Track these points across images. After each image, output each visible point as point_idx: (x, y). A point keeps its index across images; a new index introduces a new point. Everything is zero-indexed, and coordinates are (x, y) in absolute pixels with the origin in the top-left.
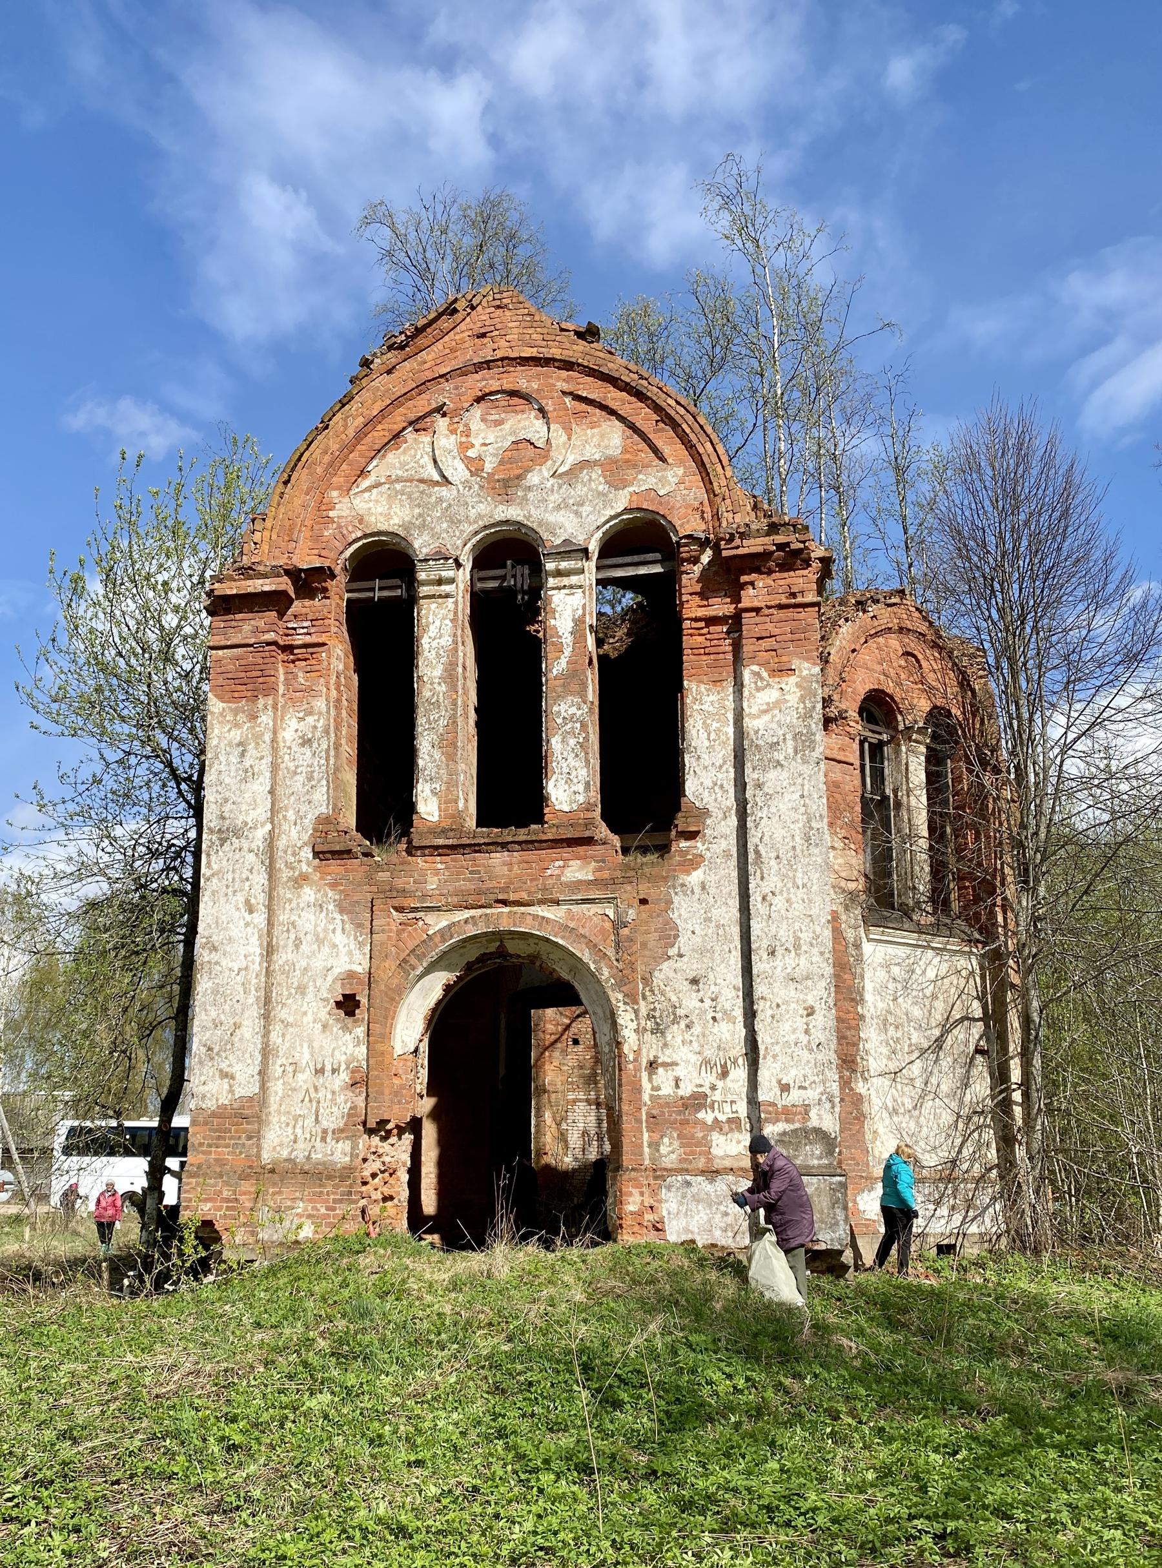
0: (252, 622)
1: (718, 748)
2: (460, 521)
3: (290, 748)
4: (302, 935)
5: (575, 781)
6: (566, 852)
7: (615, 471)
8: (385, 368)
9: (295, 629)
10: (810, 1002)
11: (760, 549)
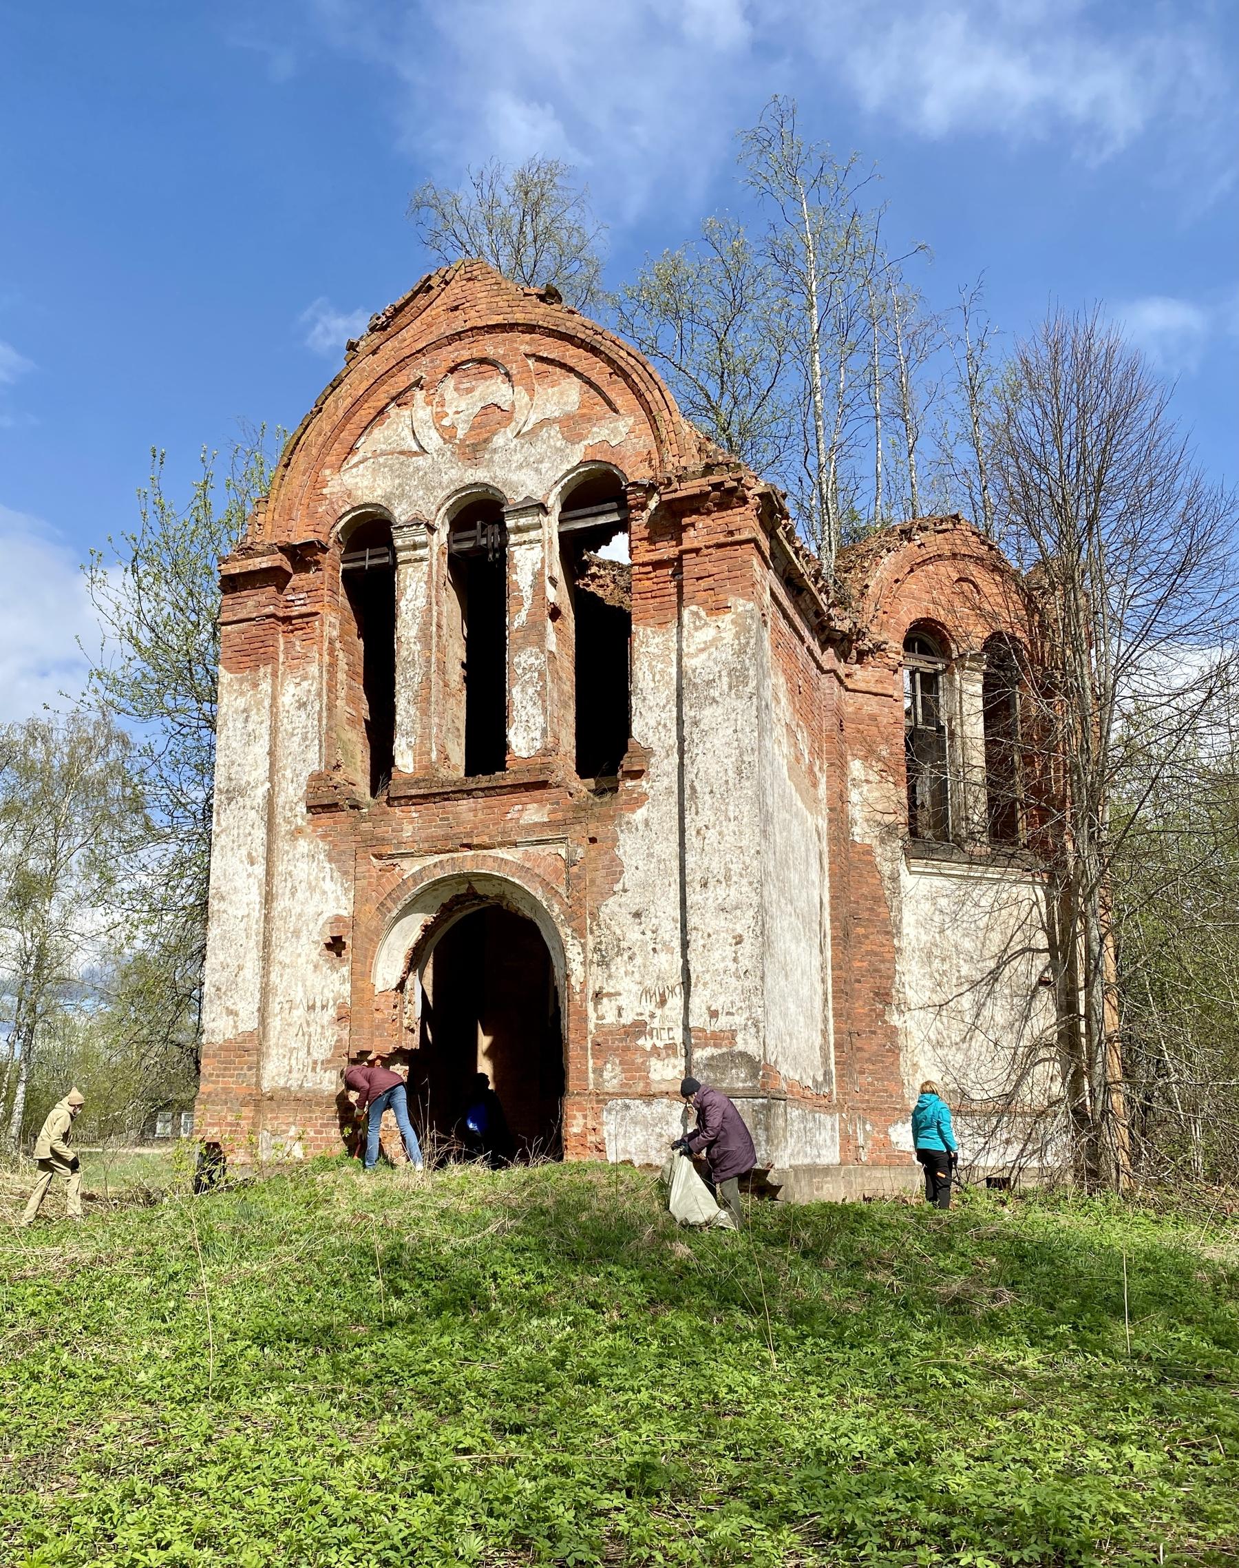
2: (434, 488)
4: (297, 884)
5: (533, 728)
6: (524, 796)
7: (572, 426)
10: (739, 931)
11: (697, 491)
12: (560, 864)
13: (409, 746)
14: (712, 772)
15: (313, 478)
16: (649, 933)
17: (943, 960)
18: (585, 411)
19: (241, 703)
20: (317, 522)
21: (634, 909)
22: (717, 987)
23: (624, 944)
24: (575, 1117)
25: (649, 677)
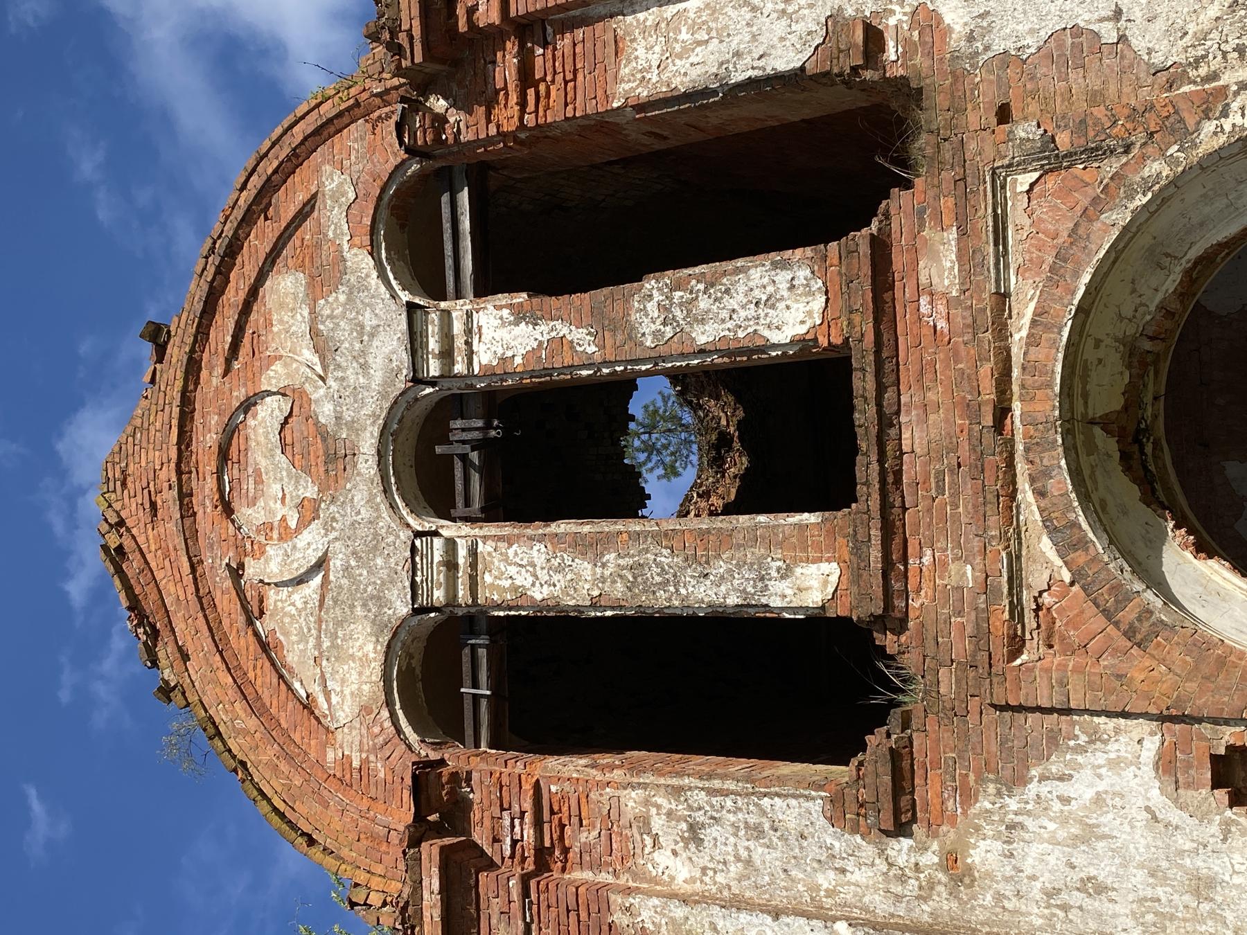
0: (494, 921)
2: (376, 535)
3: (704, 870)
4: (1076, 876)
5: (770, 289)
6: (903, 292)
8: (178, 664)
9: (514, 843)
12: (1051, 182)
13: (785, 574)
15: (332, 785)
25: (699, 54)
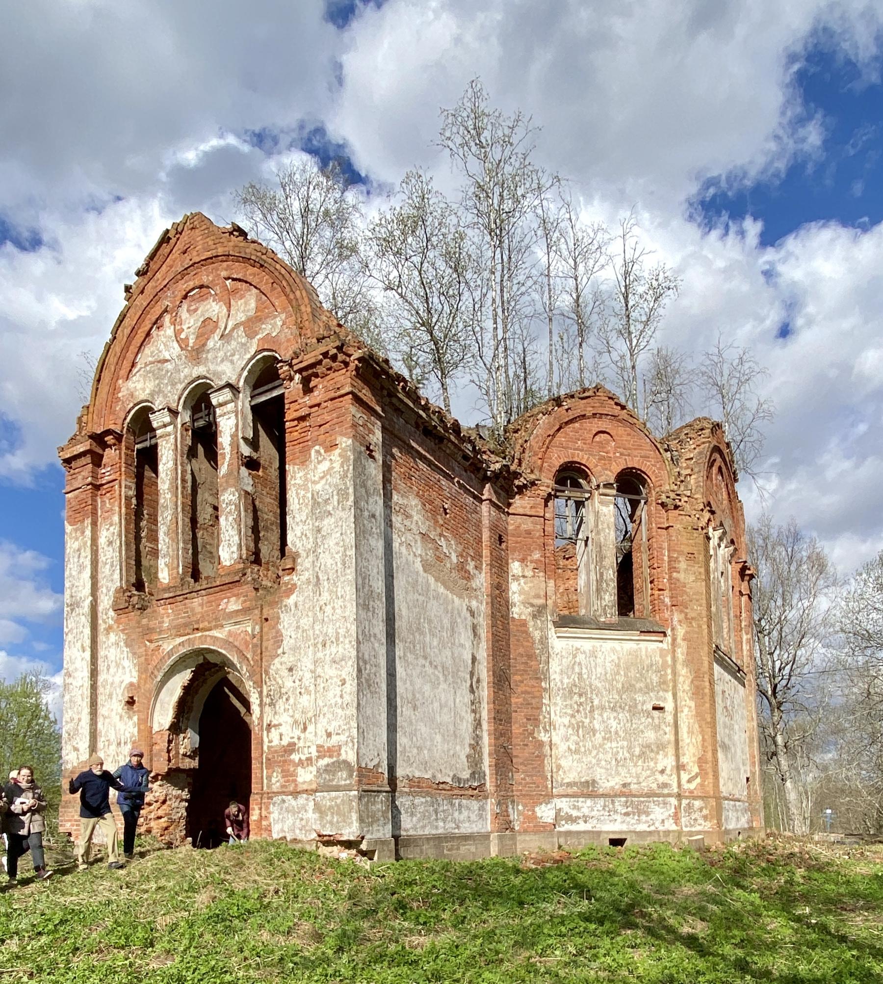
1: (304, 508)
7: (250, 326)
10: (344, 676)
12: (248, 638)
13: (166, 565)
14: (329, 565)
16: (297, 681)
17: (580, 695)
18: (259, 314)
19: (76, 545)
20: (117, 420)
21: (289, 665)
22: (330, 716)
23: (283, 690)
24: (254, 809)
25: (296, 501)
